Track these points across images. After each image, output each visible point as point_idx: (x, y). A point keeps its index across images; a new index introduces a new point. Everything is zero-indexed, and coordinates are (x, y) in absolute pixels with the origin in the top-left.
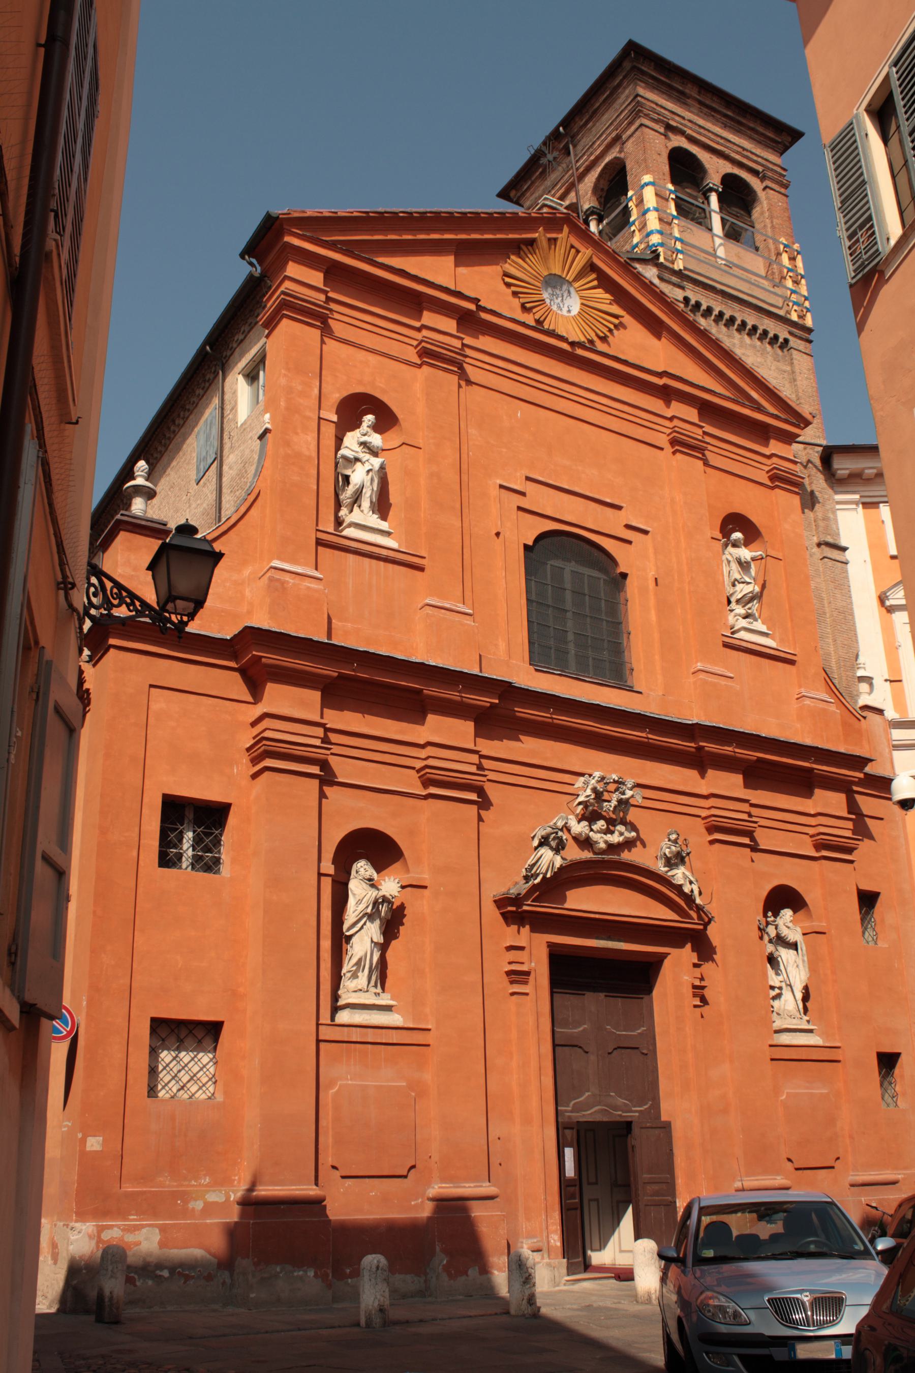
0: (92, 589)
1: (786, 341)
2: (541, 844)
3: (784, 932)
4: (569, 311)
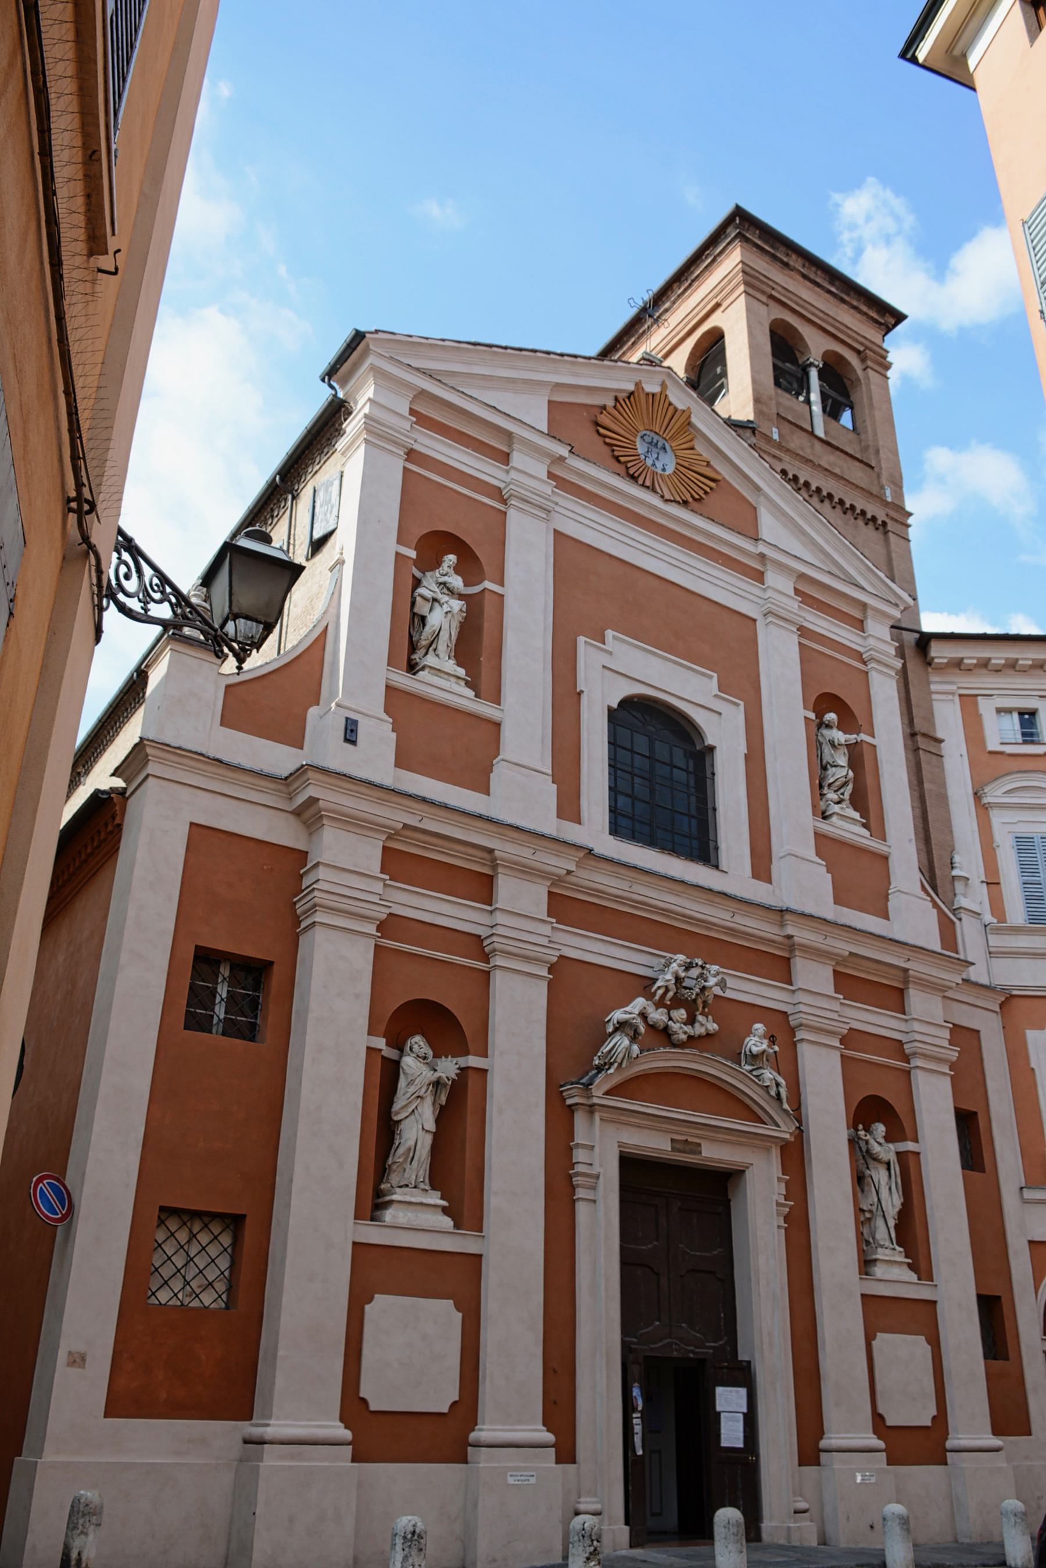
0: (123, 569)
1: (884, 524)
3: (876, 1148)
4: (664, 470)
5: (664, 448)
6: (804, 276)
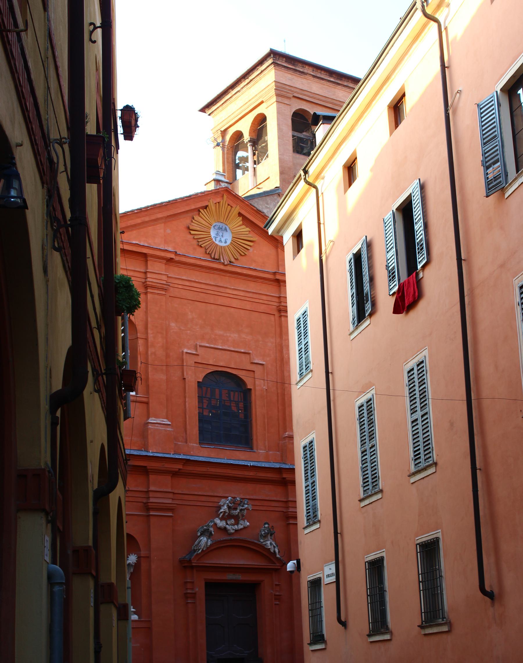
2: (201, 535)
4: (226, 242)
5: (226, 229)
6: (314, 76)
